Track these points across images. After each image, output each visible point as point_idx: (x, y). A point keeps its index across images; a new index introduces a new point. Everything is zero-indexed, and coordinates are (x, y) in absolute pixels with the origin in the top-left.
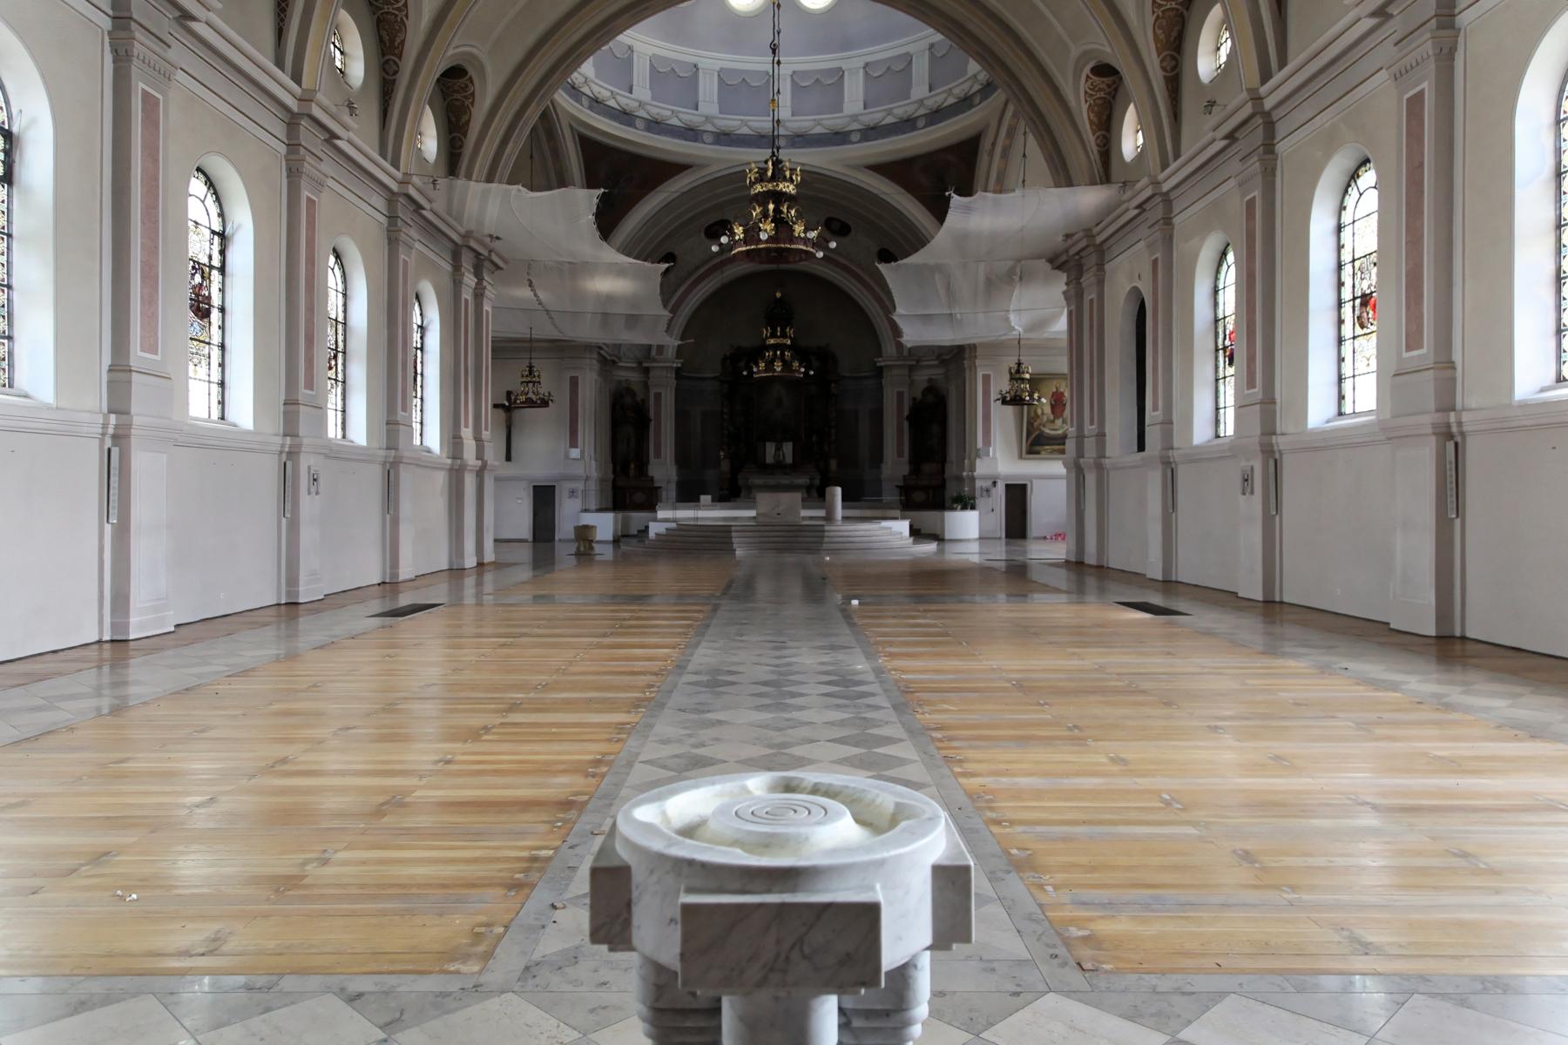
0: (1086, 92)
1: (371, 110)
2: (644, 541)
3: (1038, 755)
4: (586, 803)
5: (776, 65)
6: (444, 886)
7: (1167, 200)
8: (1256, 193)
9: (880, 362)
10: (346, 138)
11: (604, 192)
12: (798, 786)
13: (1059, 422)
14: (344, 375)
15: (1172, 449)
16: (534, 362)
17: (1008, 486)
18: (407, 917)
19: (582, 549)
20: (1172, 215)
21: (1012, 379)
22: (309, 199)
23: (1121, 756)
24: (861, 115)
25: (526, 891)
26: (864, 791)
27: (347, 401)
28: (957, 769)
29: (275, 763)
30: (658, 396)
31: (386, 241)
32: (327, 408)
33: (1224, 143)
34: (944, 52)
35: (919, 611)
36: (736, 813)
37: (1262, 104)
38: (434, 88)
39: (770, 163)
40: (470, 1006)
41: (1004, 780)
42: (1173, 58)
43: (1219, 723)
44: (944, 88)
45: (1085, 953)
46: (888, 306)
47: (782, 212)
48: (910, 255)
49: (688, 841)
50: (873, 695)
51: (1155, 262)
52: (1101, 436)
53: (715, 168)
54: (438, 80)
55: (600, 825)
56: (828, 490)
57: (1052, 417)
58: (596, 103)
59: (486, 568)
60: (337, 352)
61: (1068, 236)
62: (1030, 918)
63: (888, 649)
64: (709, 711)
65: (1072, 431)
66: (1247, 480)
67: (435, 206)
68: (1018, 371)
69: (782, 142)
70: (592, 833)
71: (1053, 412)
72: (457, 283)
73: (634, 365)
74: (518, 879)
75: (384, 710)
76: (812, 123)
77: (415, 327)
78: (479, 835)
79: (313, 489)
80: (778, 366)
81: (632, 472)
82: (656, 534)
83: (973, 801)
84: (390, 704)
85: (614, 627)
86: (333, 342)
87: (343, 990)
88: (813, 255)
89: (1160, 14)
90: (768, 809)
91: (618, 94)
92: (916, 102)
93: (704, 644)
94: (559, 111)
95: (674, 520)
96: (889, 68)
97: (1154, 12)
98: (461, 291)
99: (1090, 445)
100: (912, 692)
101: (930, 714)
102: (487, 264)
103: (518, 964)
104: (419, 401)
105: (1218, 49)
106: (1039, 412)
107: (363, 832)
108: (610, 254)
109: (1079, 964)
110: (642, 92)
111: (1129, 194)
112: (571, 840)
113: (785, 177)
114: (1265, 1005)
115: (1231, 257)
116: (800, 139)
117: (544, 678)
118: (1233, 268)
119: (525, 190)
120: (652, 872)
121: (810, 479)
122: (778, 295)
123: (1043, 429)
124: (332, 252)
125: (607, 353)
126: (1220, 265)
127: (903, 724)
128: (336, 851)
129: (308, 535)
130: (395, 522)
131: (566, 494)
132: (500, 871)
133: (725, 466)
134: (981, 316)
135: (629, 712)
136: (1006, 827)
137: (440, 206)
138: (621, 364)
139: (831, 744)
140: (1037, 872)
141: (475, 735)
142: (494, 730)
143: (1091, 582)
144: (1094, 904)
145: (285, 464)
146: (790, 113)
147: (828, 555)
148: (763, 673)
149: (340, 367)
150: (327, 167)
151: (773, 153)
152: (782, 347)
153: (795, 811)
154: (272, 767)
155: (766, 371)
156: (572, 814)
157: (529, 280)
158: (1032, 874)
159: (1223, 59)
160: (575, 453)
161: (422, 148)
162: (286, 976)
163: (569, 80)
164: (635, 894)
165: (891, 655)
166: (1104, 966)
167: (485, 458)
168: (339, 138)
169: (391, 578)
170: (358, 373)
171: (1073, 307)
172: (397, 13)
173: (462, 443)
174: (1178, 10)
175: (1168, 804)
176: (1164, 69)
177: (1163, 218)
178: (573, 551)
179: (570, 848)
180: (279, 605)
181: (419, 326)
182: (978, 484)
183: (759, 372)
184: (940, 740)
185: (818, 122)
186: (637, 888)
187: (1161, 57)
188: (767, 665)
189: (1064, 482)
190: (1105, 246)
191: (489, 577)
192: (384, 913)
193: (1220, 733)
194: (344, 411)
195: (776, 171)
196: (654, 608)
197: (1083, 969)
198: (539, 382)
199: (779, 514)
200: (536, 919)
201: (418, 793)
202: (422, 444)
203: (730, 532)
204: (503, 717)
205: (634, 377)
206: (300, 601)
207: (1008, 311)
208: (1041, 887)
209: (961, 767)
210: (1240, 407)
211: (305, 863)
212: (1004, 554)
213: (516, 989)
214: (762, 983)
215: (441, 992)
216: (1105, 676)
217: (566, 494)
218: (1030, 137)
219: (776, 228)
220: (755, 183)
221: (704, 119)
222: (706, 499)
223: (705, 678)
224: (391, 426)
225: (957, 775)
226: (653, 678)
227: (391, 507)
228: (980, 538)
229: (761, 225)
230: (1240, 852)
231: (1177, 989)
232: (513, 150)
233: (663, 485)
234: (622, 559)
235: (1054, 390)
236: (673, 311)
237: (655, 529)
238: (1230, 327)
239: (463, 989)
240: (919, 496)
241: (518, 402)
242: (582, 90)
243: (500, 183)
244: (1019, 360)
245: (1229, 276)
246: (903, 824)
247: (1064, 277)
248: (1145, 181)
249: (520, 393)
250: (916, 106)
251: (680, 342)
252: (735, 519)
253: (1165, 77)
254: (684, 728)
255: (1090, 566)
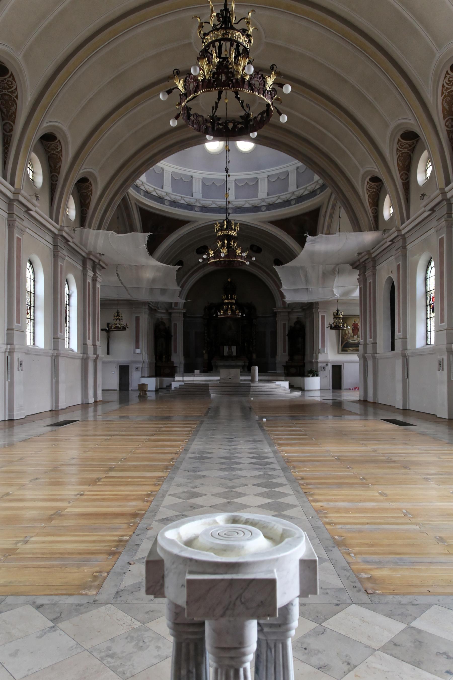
0: (367, 189)
1: (45, 198)
2: (169, 391)
3: (346, 492)
4: (144, 514)
5: (228, 177)
6: (80, 554)
7: (404, 238)
8: (444, 235)
9: (275, 310)
10: (34, 210)
11: (150, 234)
12: (239, 520)
13: (356, 337)
14: (34, 317)
15: (407, 350)
16: (120, 310)
17: (333, 366)
18: (63, 568)
19: (141, 394)
20: (406, 245)
21: (334, 318)
22: (18, 238)
23: (384, 492)
24: (266, 199)
25: (117, 556)
26: (268, 523)
27: (35, 328)
28: (311, 499)
29: (4, 495)
30: (175, 325)
31: (53, 257)
32: (26, 332)
33: (429, 212)
34: (303, 171)
35: (293, 424)
36: (211, 534)
37: (446, 196)
38: (74, 187)
39: (225, 222)
40: (92, 610)
41: (332, 503)
42: (406, 174)
43: (429, 477)
44: (303, 187)
45: (369, 585)
46: (279, 285)
47: (231, 244)
48: (289, 262)
49: (189, 549)
50: (272, 463)
51: (399, 266)
52: (375, 344)
53: (200, 223)
54: (76, 184)
55: (150, 525)
56: (252, 368)
57: (352, 335)
58: (147, 194)
59: (98, 403)
60: (31, 306)
61: (359, 254)
62: (344, 569)
63: (279, 442)
64: (199, 471)
65: (362, 341)
66: (440, 364)
67: (74, 240)
68: (337, 314)
69: (231, 211)
70: (147, 528)
71: (353, 332)
72: (85, 275)
73: (164, 311)
74: (114, 550)
75: (52, 470)
76: (245, 202)
77: (66, 295)
78: (95, 530)
79: (20, 368)
80: (229, 312)
81: (164, 360)
82: (175, 388)
83: (318, 513)
84: (56, 468)
85: (156, 431)
86: (29, 302)
87: (34, 603)
88: (245, 263)
89: (400, 154)
90: (225, 532)
91: (157, 189)
92: (290, 193)
93: (196, 439)
94: (130, 197)
95: (183, 381)
96: (278, 178)
97: (397, 154)
98: (86, 278)
99: (370, 347)
100: (290, 462)
101: (298, 472)
102: (98, 266)
103: (114, 591)
104: (68, 328)
105: (426, 170)
106: (347, 332)
107: (43, 528)
108: (153, 262)
109: (366, 590)
110: (168, 188)
111: (387, 235)
112: (137, 532)
113: (232, 228)
114: (450, 610)
115: (433, 264)
116: (239, 209)
117: (124, 455)
118: (434, 269)
119: (115, 233)
120: (173, 563)
121: (244, 363)
122: (229, 280)
123: (349, 340)
124: (28, 261)
125: (152, 305)
126: (428, 267)
127: (286, 477)
128: (31, 537)
129: (18, 389)
130: (57, 383)
131: (134, 370)
132: (105, 546)
133: (206, 356)
134: (320, 289)
135: (163, 471)
136: (333, 526)
137: (77, 240)
138: (159, 311)
139: (254, 486)
140: (347, 547)
141: (94, 482)
142: (102, 480)
143: (371, 410)
144: (373, 562)
145: (7, 357)
146: (234, 198)
147: (252, 397)
148: (223, 453)
149: (32, 313)
150: (26, 223)
151: (227, 217)
152: (231, 304)
153: (238, 533)
154: (2, 497)
155: (224, 315)
156: (138, 520)
157: (117, 273)
158: (345, 548)
159: (429, 175)
160: (138, 351)
161: (69, 214)
162: (9, 596)
163: (135, 183)
164: (166, 573)
165: (281, 445)
166: (377, 592)
167: (98, 354)
168: (31, 210)
169: (55, 408)
170: (40, 316)
171: (362, 286)
172: (57, 154)
173: (87, 347)
174: (408, 153)
175: (405, 514)
176: (402, 179)
177: (402, 246)
178: (138, 395)
179: (137, 535)
180: (5, 420)
181: (67, 294)
182: (320, 365)
183: (221, 315)
184: (303, 485)
185: (247, 202)
186: (167, 570)
187: (401, 174)
188: (225, 449)
189: (358, 364)
190: (376, 259)
191: (99, 408)
192: (53, 566)
193: (429, 481)
194: (34, 333)
195: (228, 226)
196: (174, 422)
197: (368, 593)
198: (122, 319)
199: (230, 379)
200: (122, 569)
201: (68, 510)
202: (69, 347)
203: (208, 387)
204: (106, 473)
205: (165, 317)
206: (15, 419)
207: (333, 287)
208: (349, 554)
209: (312, 497)
210: (437, 331)
211: (17, 543)
212: (331, 397)
213: (112, 603)
214: (223, 615)
215: (79, 604)
216: (377, 454)
217: (134, 370)
218: (342, 209)
219: (228, 251)
220: (218, 231)
221: (196, 200)
222: (197, 372)
223: (197, 455)
224: (55, 340)
225: (310, 501)
226: (174, 455)
227: (55, 376)
228: (321, 389)
229: (221, 250)
230: (438, 538)
231: (410, 602)
232: (110, 215)
233: (178, 365)
234: (159, 399)
235: (354, 323)
236: (182, 287)
237: (174, 385)
238: (432, 295)
239: (88, 602)
240: (293, 370)
241: (112, 328)
242: (140, 187)
243: (104, 230)
244: (338, 309)
245: (432, 272)
246: (286, 540)
247: (357, 272)
248: (394, 229)
249: (113, 324)
250: (290, 195)
251: (185, 301)
252: (210, 381)
253: (402, 183)
254: (188, 479)
255: (370, 402)
